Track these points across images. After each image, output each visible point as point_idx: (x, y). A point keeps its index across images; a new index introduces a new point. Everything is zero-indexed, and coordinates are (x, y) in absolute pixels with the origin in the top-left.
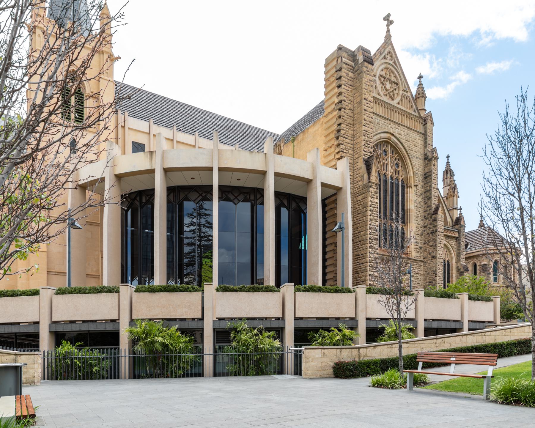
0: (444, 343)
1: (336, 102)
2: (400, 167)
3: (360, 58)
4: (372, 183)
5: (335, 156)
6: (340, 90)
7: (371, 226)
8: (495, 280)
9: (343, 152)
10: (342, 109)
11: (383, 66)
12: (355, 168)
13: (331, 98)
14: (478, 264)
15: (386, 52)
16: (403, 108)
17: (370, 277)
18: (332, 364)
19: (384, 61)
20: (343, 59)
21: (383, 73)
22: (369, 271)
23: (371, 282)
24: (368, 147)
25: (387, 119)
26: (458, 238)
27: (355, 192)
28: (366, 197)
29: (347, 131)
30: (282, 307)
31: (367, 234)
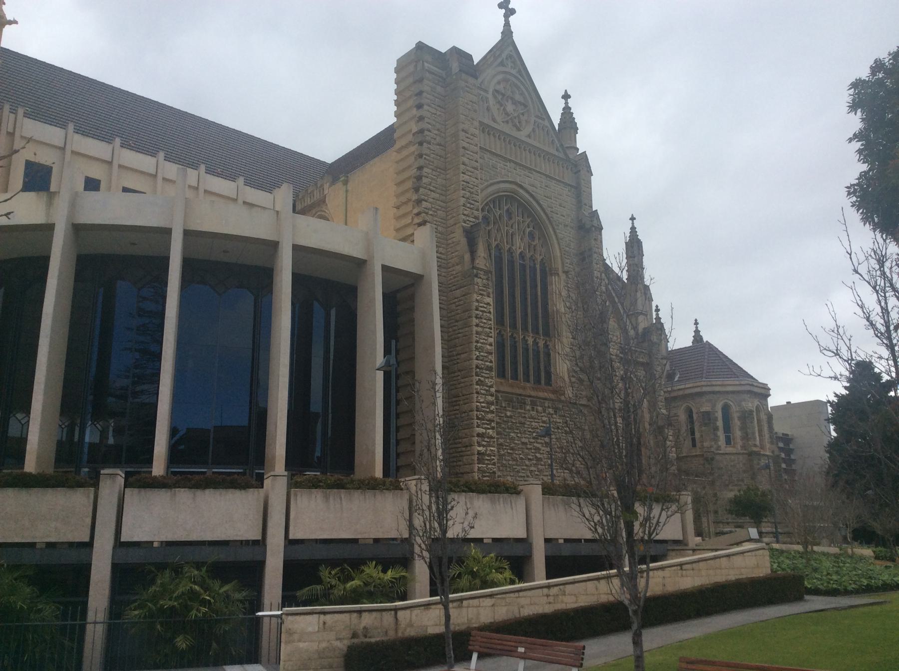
0: (565, 595)
1: (414, 131)
2: (537, 238)
3: (455, 66)
4: (478, 269)
5: (413, 219)
6: (421, 113)
7: (479, 345)
8: (728, 441)
9: (427, 213)
10: (425, 144)
11: (500, 77)
12: (450, 242)
13: (405, 123)
14: (694, 411)
15: (504, 56)
16: (538, 145)
17: (480, 439)
18: (342, 646)
19: (504, 69)
20: (426, 64)
21: (500, 87)
22: (477, 427)
23: (480, 449)
24: (471, 208)
25: (510, 161)
26: (648, 364)
27: (450, 282)
28: (469, 294)
29: (434, 179)
30: (261, 522)
31: (471, 359)
